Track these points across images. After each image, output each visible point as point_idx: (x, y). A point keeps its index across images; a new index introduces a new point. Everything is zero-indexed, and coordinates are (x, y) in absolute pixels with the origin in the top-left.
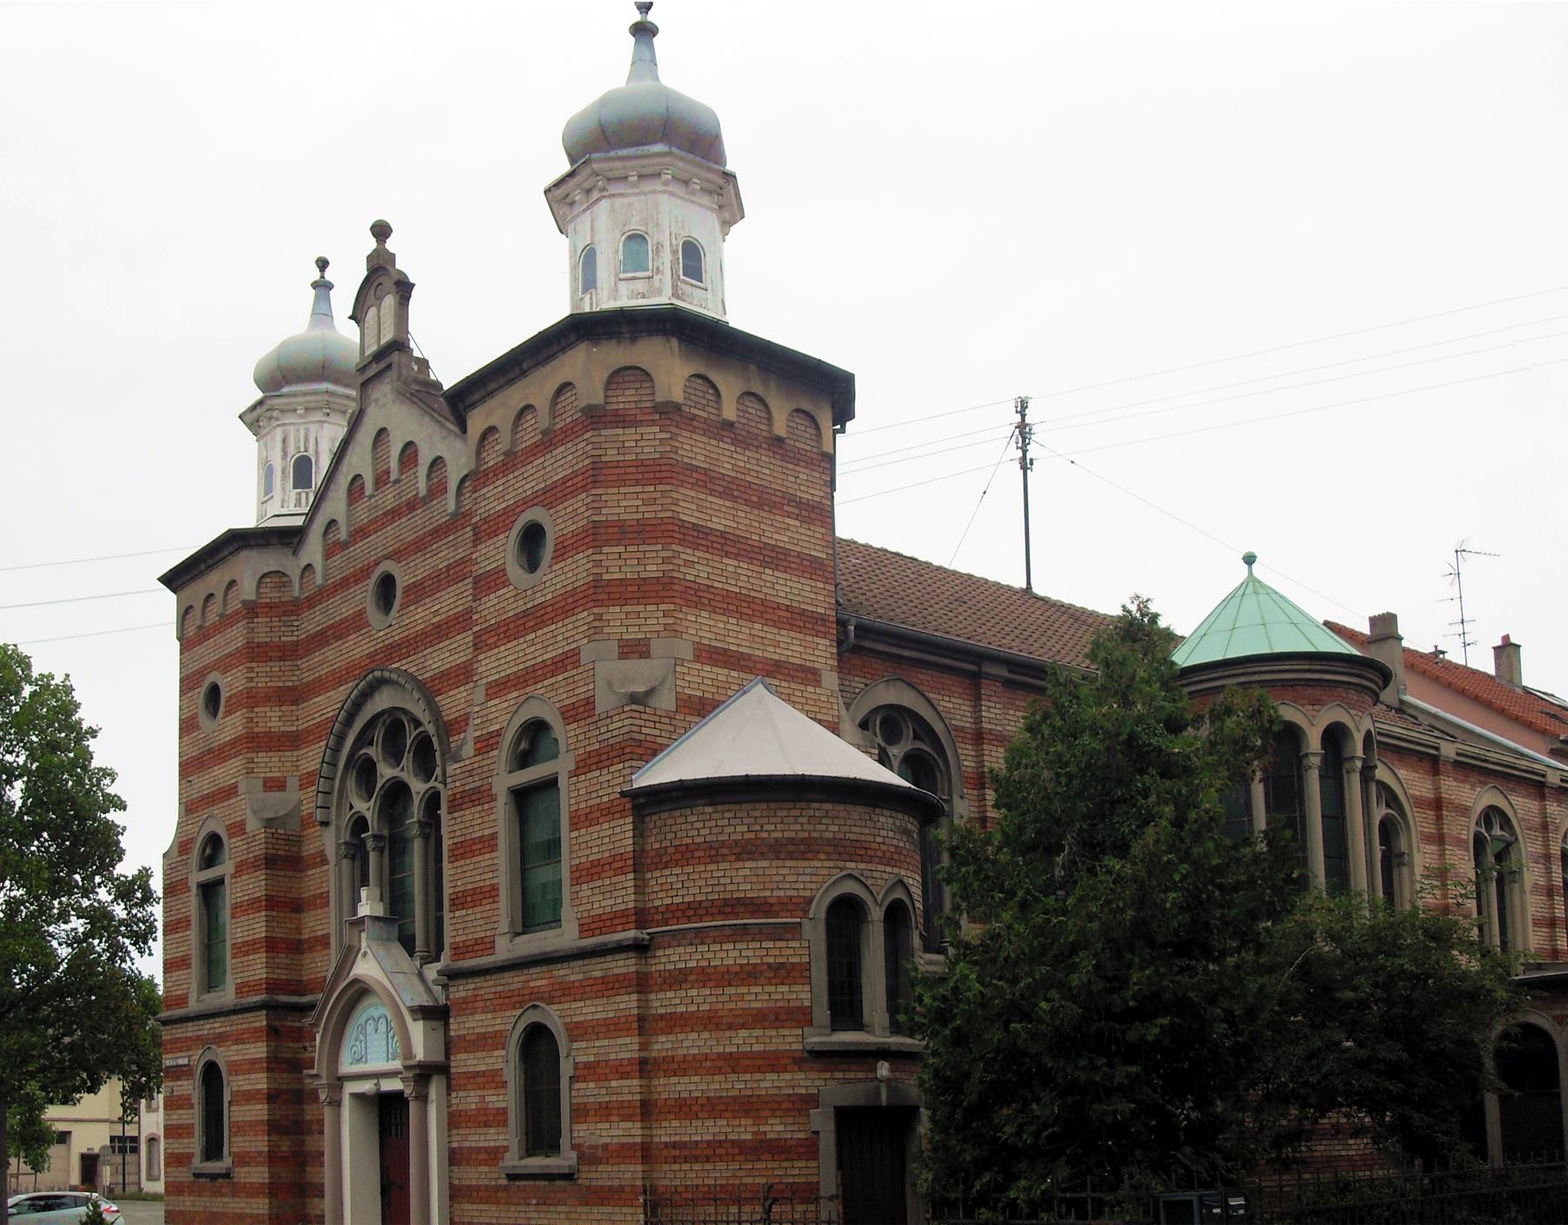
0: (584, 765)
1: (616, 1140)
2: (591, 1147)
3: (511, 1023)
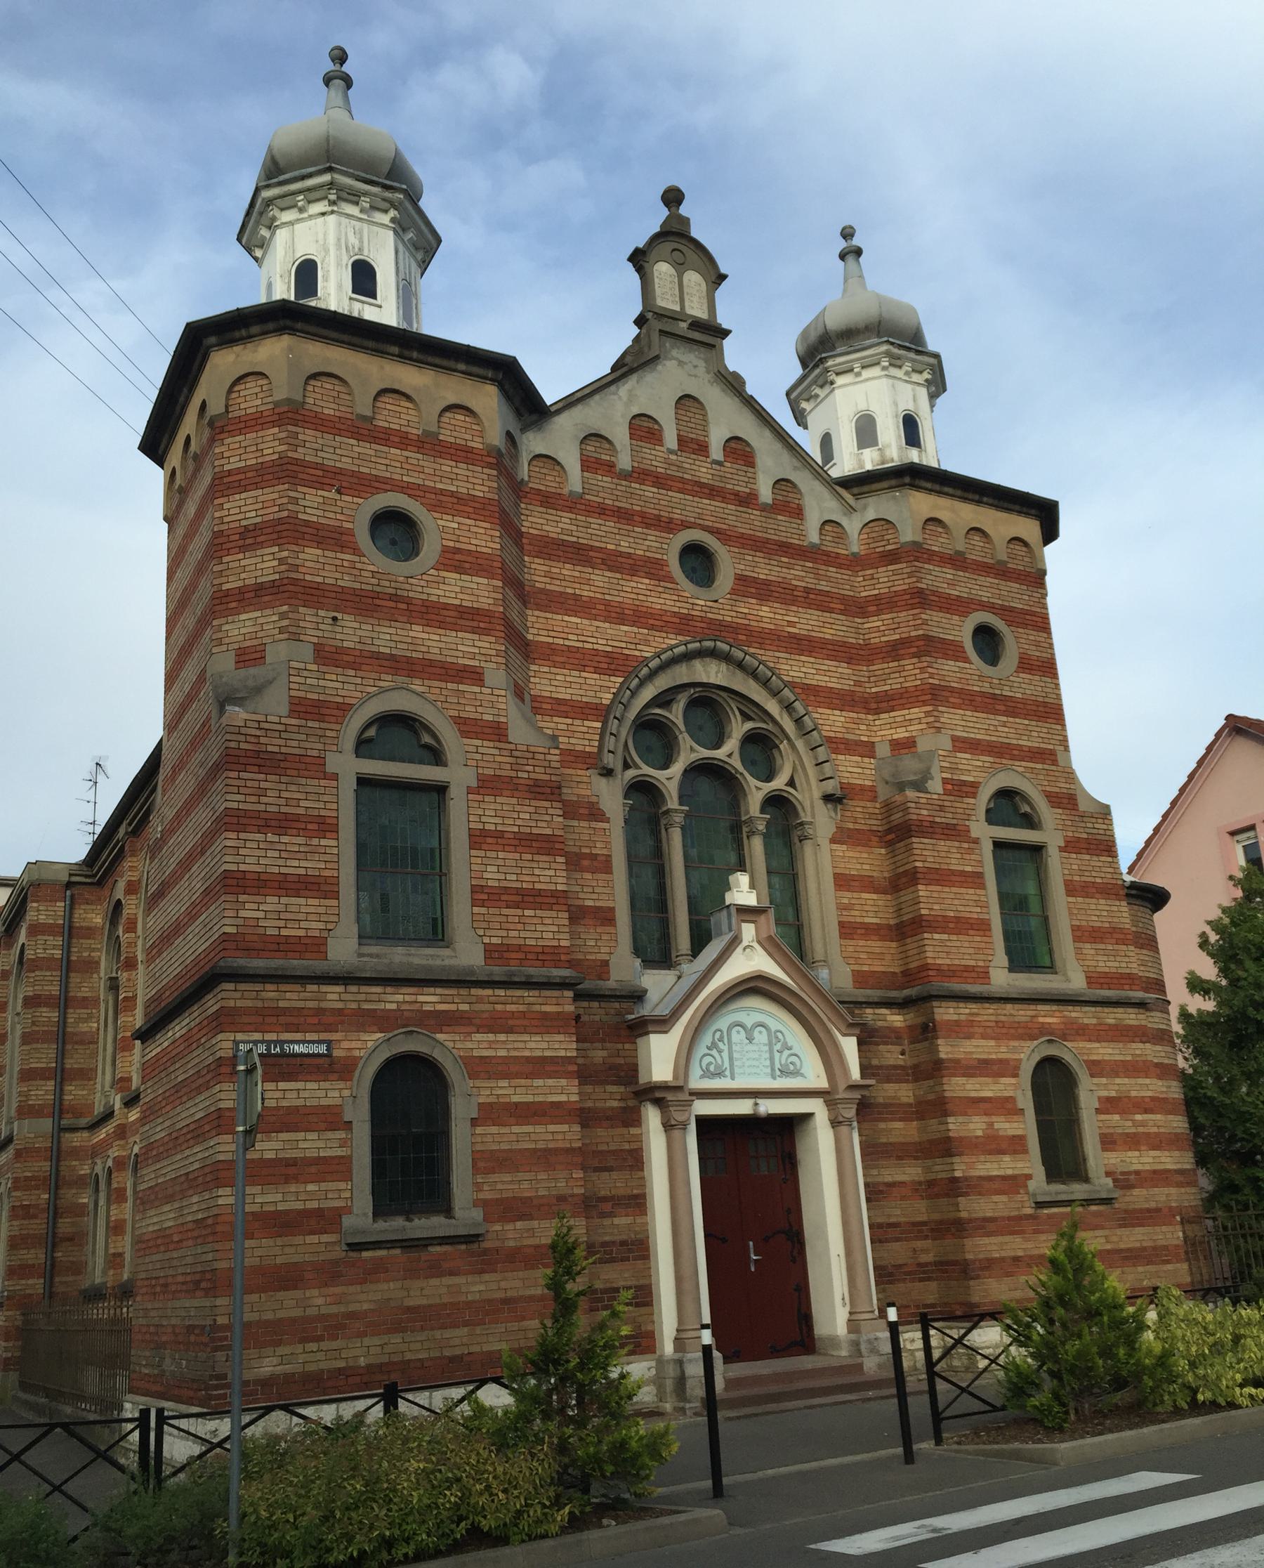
0: (487, 785)
1: (1147, 1167)
2: (1123, 1173)
3: (1028, 1054)
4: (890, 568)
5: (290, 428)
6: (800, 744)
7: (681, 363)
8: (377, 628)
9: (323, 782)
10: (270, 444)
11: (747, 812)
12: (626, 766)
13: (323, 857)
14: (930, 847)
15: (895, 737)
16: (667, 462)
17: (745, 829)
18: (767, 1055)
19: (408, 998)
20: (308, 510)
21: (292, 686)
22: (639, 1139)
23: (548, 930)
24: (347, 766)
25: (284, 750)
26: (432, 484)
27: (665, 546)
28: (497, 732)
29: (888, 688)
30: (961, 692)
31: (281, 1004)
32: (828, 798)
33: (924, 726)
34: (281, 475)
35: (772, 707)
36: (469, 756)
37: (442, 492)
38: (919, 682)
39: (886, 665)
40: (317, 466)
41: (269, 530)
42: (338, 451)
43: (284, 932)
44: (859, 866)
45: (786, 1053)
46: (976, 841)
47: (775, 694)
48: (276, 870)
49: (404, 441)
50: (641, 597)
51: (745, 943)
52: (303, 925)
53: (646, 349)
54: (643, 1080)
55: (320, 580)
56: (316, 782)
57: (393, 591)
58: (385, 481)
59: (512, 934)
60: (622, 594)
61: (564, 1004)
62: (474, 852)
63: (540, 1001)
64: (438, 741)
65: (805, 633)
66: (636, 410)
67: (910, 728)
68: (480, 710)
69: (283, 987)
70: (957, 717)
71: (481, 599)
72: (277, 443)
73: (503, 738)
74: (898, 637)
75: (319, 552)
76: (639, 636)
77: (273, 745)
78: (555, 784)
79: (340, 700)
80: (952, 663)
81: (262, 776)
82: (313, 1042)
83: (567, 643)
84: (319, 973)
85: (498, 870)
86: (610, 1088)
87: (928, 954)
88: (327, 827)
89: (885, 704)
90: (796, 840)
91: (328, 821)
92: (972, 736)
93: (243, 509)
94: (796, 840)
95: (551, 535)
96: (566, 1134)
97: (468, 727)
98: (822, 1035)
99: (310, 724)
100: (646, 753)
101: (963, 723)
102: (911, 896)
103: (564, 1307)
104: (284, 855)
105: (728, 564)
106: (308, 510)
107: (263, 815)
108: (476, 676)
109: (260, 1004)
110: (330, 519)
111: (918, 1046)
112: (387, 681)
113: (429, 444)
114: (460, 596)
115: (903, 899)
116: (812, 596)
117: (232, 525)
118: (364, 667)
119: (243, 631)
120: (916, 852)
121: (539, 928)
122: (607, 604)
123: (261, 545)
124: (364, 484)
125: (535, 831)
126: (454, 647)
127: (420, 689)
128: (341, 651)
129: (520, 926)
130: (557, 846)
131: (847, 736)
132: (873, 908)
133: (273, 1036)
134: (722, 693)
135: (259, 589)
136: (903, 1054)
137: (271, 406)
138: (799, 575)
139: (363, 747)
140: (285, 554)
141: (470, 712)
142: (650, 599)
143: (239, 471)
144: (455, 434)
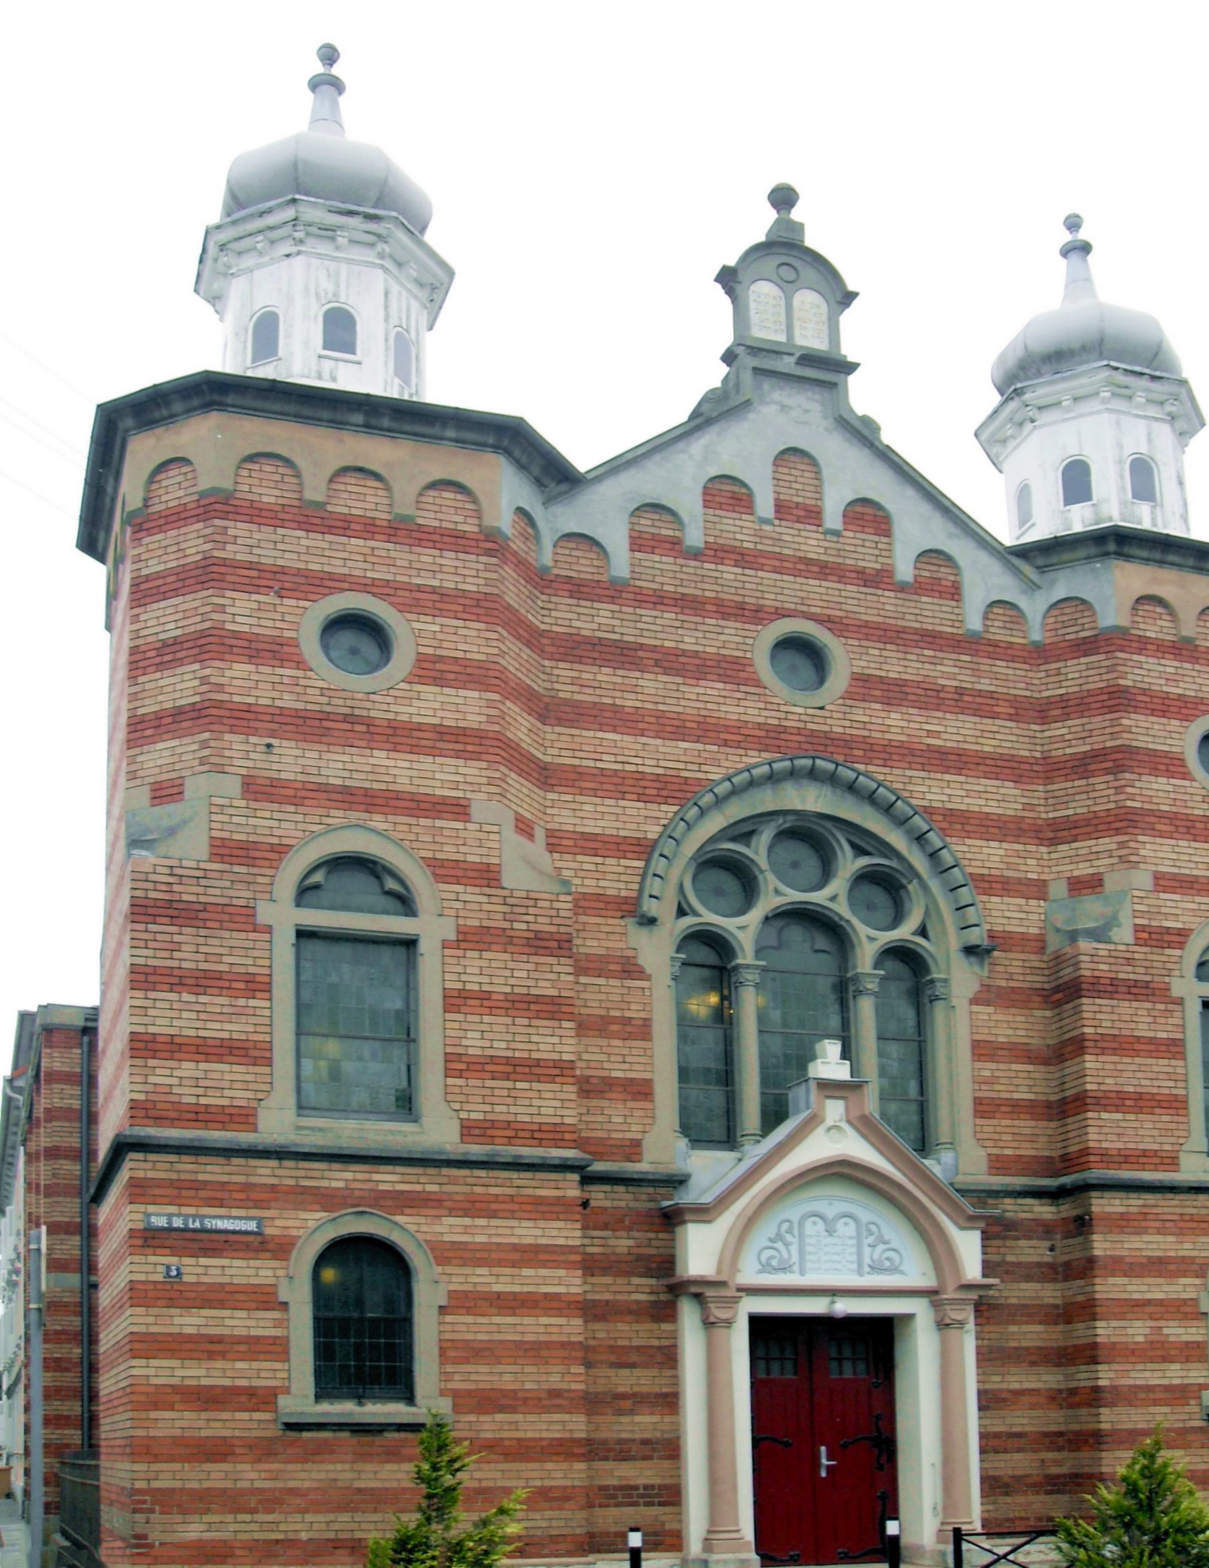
0: (470, 939)
4: (1083, 660)
5: (217, 522)
6: (934, 885)
7: (784, 408)
8: (326, 756)
9: (252, 936)
10: (192, 543)
11: (855, 967)
12: (681, 912)
13: (253, 1020)
14: (1109, 1009)
15: (1076, 873)
16: (759, 534)
17: (851, 988)
18: (854, 1250)
19: (359, 1176)
20: (238, 619)
21: (214, 825)
22: (674, 1336)
23: (550, 1104)
24: (282, 915)
25: (202, 899)
26: (406, 579)
27: (750, 641)
28: (488, 876)
29: (1070, 812)
30: (1173, 818)
31: (201, 1177)
32: (970, 950)
33: (1115, 860)
34: (203, 578)
35: (896, 839)
36: (446, 904)
37: (420, 588)
38: (1112, 806)
39: (1070, 784)
40: (250, 566)
41: (190, 644)
42: (280, 546)
43: (203, 1101)
44: (1010, 1032)
45: (882, 1247)
46: (1180, 1002)
47: (901, 822)
48: (193, 1033)
49: (369, 528)
50: (709, 706)
51: (829, 1122)
52: (227, 1093)
53: (733, 393)
54: (679, 1271)
55: (251, 700)
56: (243, 935)
57: (348, 711)
58: (343, 578)
59: (498, 1108)
60: (683, 703)
61: (570, 1187)
62: (449, 1016)
63: (534, 1183)
64: (406, 887)
65: (954, 745)
66: (714, 471)
67: (1095, 863)
68: (462, 849)
69: (202, 1159)
70: (1165, 848)
71: (469, 717)
72: (201, 541)
73: (493, 883)
74: (1087, 748)
75: (252, 668)
76: (704, 755)
77: (189, 893)
78: (565, 937)
79: (275, 841)
80: (1164, 780)
81: (174, 929)
82: (240, 1218)
83: (599, 764)
84: (244, 1146)
85: (483, 1036)
86: (636, 1280)
87: (1091, 1137)
88: (258, 986)
89: (1065, 833)
90: (926, 1001)
91: (259, 979)
92: (1187, 872)
93: (162, 620)
94: (926, 1001)
95: (583, 632)
96: (572, 1328)
97: (446, 871)
98: (929, 1229)
99: (236, 869)
100: (712, 896)
101: (1175, 856)
102: (1075, 1069)
103: (438, 1502)
104: (203, 1016)
105: (845, 658)
106: (238, 619)
107: (176, 972)
108: (459, 810)
109: (174, 1176)
110: (266, 627)
111: (1071, 1241)
112: (337, 817)
113: (400, 530)
114: (440, 713)
115: (1067, 1071)
116: (966, 698)
117: (149, 639)
118: (307, 802)
119: (160, 762)
120: (1085, 1015)
121: (535, 1102)
122: (660, 715)
123: (181, 662)
124: (314, 584)
125: (534, 991)
126: (430, 775)
127: (382, 826)
128: (274, 783)
129: (510, 1101)
130: (565, 1009)
131: (1007, 873)
132: (1023, 1082)
133: (191, 1210)
134: (824, 823)
135: (178, 713)
136: (1051, 1250)
137: (195, 497)
138: (949, 671)
139: (305, 893)
140: (207, 671)
141: (449, 852)
142: (723, 708)
143: (158, 575)
144: (440, 516)
